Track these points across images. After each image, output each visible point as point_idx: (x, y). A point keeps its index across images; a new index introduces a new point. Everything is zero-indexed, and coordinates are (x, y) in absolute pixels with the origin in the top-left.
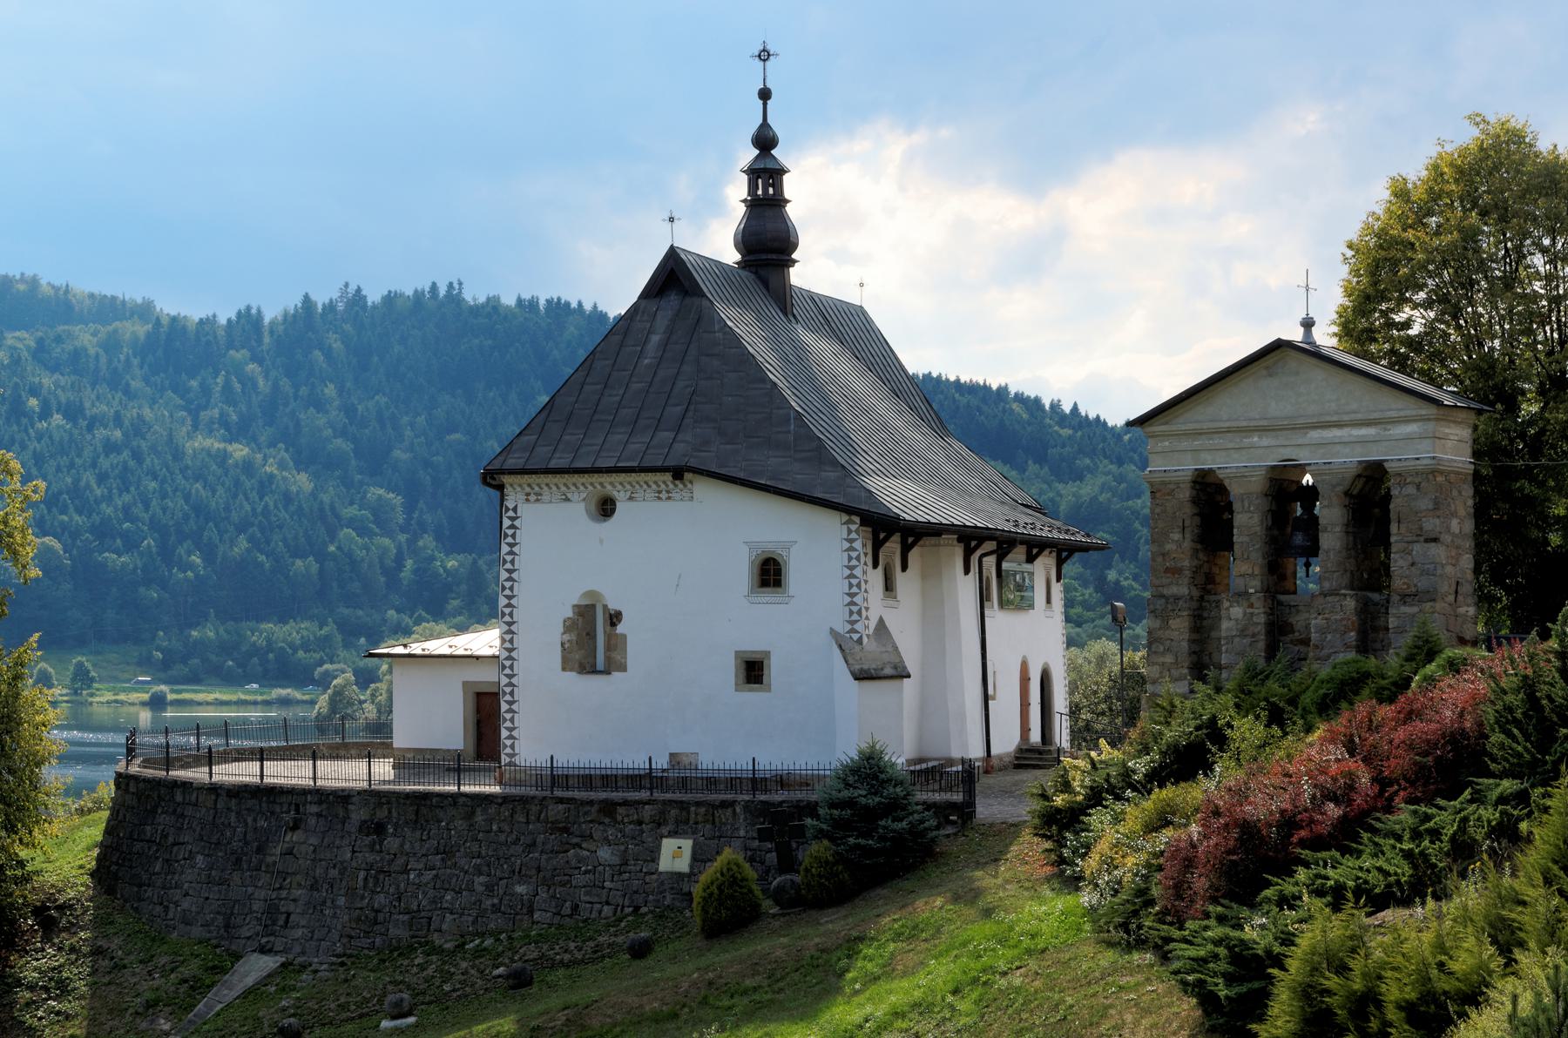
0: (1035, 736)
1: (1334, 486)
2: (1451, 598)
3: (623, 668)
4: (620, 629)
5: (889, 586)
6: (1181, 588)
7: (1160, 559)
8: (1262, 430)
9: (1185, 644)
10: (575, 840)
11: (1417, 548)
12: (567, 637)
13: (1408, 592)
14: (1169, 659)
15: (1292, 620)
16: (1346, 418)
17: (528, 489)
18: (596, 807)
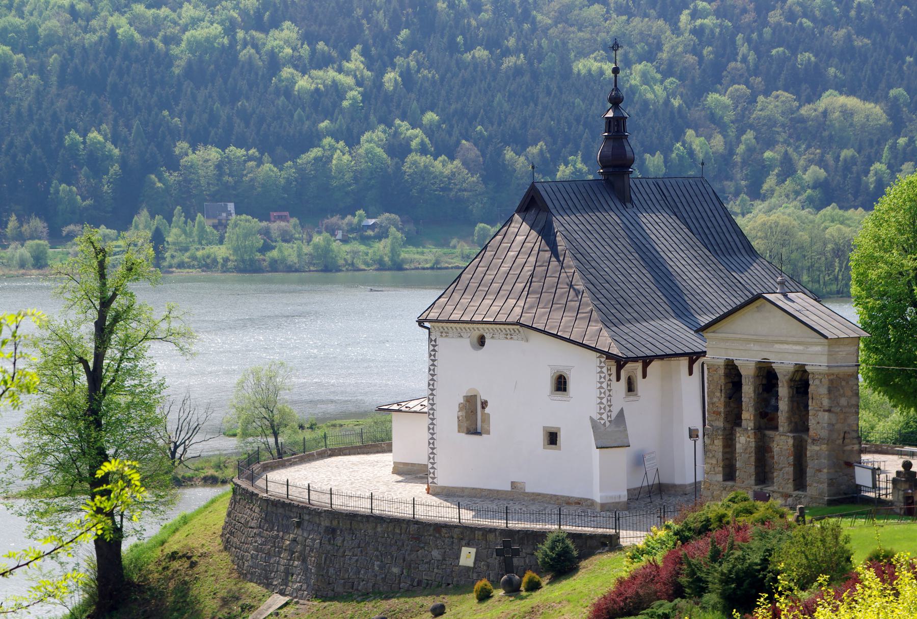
2: (841, 441)
3: (489, 433)
4: (487, 410)
5: (631, 387)
6: (720, 424)
8: (756, 341)
9: (721, 454)
10: (422, 545)
11: (820, 414)
12: (460, 414)
16: (790, 339)
18: (432, 529)
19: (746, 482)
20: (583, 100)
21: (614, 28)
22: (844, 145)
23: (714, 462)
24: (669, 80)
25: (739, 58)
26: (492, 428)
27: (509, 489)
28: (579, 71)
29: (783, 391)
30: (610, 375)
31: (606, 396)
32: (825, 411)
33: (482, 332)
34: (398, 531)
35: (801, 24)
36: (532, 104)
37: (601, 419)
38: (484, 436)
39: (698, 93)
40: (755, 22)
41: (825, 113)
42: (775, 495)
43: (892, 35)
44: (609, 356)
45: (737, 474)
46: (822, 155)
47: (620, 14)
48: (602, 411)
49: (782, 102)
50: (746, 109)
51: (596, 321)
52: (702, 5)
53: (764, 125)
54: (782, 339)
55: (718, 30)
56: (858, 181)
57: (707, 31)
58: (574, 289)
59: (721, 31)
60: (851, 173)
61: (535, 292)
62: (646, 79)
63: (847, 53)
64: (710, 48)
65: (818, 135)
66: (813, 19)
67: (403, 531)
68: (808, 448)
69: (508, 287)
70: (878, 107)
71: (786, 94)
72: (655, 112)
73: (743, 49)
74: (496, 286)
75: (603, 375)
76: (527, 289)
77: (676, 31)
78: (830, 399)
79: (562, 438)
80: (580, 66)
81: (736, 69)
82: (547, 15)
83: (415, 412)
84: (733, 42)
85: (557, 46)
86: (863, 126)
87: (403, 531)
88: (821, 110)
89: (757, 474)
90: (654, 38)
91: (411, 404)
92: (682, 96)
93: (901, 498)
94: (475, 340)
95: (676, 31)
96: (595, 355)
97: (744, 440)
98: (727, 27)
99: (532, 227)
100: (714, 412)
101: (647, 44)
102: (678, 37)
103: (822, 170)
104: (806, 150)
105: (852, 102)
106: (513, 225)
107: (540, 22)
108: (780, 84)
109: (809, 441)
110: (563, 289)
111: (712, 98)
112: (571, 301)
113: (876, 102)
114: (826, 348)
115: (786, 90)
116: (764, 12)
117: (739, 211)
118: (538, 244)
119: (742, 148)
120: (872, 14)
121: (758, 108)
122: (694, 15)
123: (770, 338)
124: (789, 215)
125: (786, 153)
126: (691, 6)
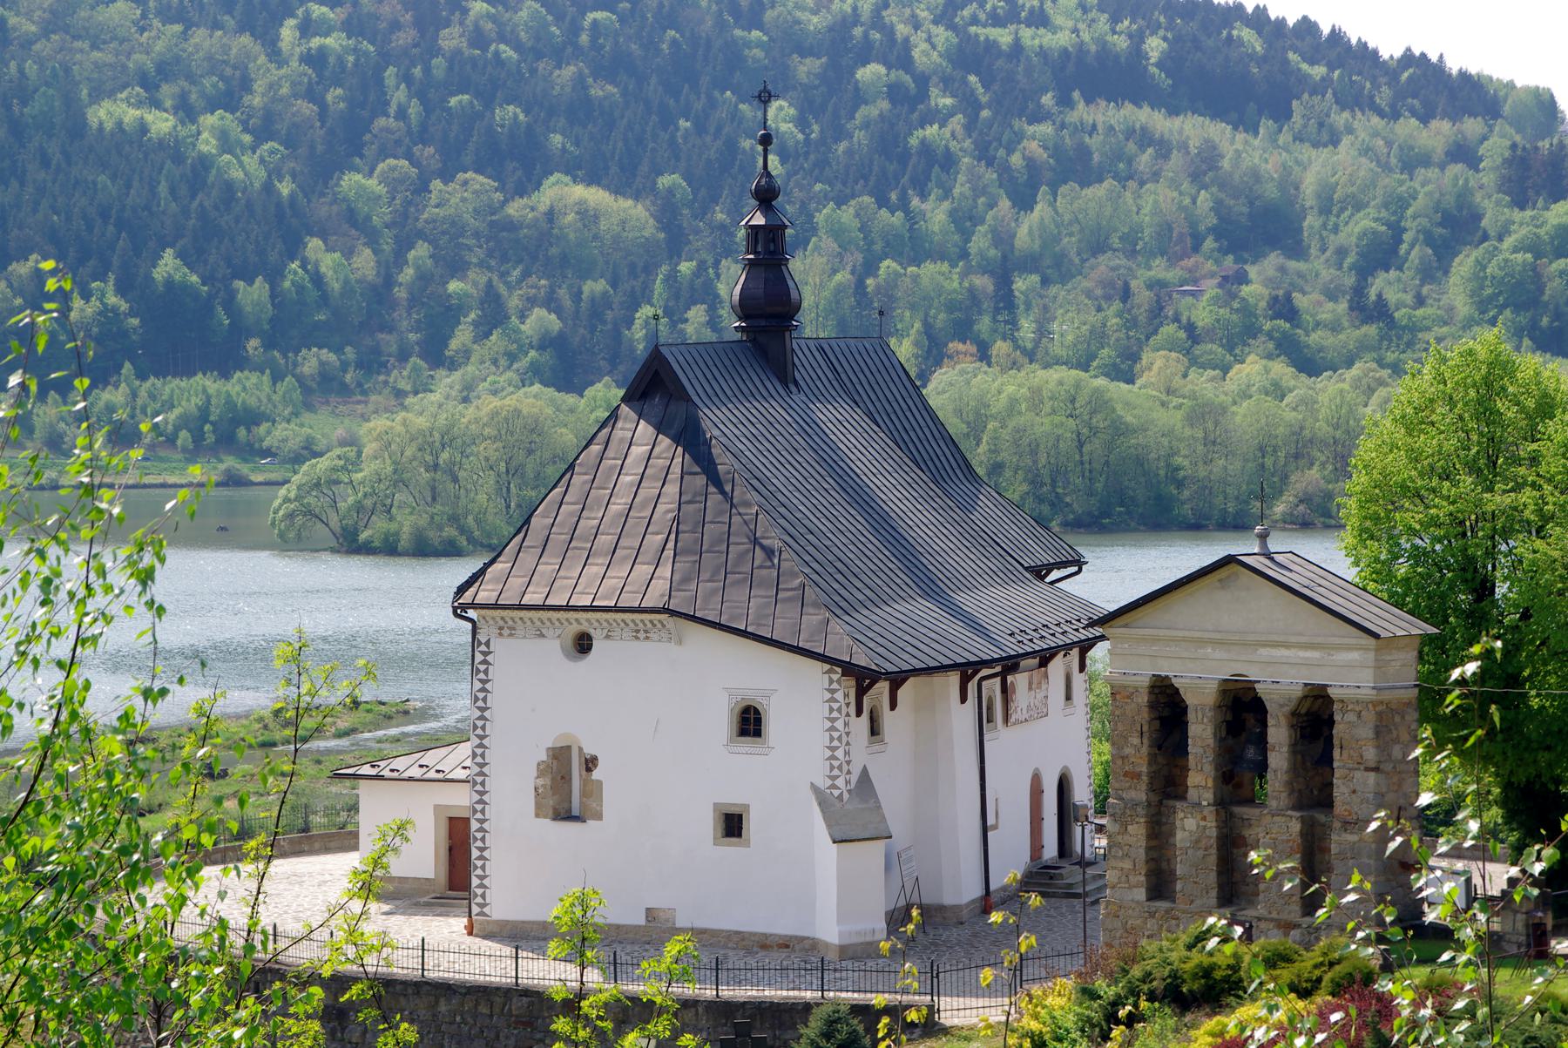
0: (1050, 850)
1: (1282, 706)
3: (599, 816)
4: (596, 774)
5: (875, 730)
6: (1140, 793)
7: (1119, 762)
9: (1142, 851)
10: (538, 1036)
11: (1358, 774)
12: (540, 782)
13: (1349, 819)
14: (1127, 865)
15: (1246, 833)
16: (1293, 639)
17: (501, 623)
19: (1198, 902)
20: (113, 178)
21: (159, 46)
22: (586, 273)
23: (1127, 865)
24: (265, 147)
25: (392, 110)
26: (607, 811)
27: (641, 920)
28: (101, 123)
29: (1279, 734)
30: (848, 705)
31: (837, 741)
32: (1367, 769)
33: (585, 627)
34: (484, 1010)
35: (497, 54)
36: (15, 184)
37: (834, 787)
38: (590, 822)
39: (322, 171)
40: (415, 46)
41: (551, 215)
42: (1263, 925)
43: (654, 80)
44: (849, 669)
45: (1179, 887)
46: (552, 291)
47: (168, 20)
48: (836, 772)
49: (476, 192)
50: (410, 203)
51: (815, 605)
52: (318, 10)
53: (443, 233)
54: (1276, 638)
55: (351, 58)
56: (617, 336)
57: (332, 60)
58: (763, 547)
59: (357, 60)
60: (604, 323)
61: (687, 552)
62: (226, 143)
63: (580, 110)
64: (339, 91)
65: (542, 252)
66: (518, 47)
67: (497, 1010)
68: (1334, 837)
69: (631, 542)
70: (640, 206)
71: (481, 178)
72: (249, 206)
73: (399, 95)
74: (605, 540)
75: (835, 706)
76: (671, 544)
77: (275, 55)
78: (1378, 747)
79: (752, 826)
80: (102, 113)
81: (387, 130)
82: (29, 15)
83: (410, 779)
84: (380, 82)
85: (54, 75)
86: (616, 239)
87: (497, 1010)
88: (542, 208)
89: (1221, 887)
90: (235, 68)
91: (399, 764)
92: (294, 176)
93: (1520, 926)
94: (569, 642)
95: (275, 55)
96: (818, 667)
97: (1193, 826)
98: (366, 54)
99: (660, 428)
100: (1126, 775)
101: (222, 78)
102: (279, 68)
103: (553, 317)
104: (520, 281)
105: (595, 196)
106: (619, 424)
107: (14, 29)
108: (468, 159)
109: (1337, 825)
110: (740, 545)
111: (351, 181)
112: (760, 567)
113: (637, 197)
114: (1371, 655)
115: (478, 171)
116: (432, 29)
117: (409, 388)
118: (678, 460)
119: (408, 274)
120: (617, 43)
121: (433, 202)
122: (307, 28)
123: (1251, 637)
124: (535, 396)
125: (490, 284)
126: (300, 12)
